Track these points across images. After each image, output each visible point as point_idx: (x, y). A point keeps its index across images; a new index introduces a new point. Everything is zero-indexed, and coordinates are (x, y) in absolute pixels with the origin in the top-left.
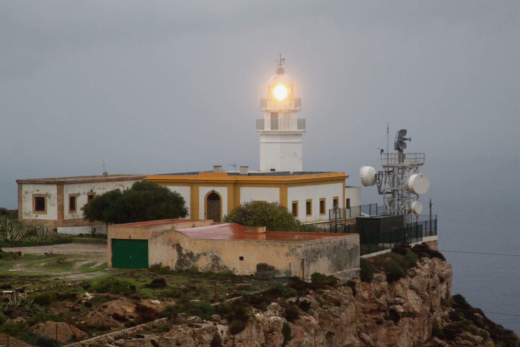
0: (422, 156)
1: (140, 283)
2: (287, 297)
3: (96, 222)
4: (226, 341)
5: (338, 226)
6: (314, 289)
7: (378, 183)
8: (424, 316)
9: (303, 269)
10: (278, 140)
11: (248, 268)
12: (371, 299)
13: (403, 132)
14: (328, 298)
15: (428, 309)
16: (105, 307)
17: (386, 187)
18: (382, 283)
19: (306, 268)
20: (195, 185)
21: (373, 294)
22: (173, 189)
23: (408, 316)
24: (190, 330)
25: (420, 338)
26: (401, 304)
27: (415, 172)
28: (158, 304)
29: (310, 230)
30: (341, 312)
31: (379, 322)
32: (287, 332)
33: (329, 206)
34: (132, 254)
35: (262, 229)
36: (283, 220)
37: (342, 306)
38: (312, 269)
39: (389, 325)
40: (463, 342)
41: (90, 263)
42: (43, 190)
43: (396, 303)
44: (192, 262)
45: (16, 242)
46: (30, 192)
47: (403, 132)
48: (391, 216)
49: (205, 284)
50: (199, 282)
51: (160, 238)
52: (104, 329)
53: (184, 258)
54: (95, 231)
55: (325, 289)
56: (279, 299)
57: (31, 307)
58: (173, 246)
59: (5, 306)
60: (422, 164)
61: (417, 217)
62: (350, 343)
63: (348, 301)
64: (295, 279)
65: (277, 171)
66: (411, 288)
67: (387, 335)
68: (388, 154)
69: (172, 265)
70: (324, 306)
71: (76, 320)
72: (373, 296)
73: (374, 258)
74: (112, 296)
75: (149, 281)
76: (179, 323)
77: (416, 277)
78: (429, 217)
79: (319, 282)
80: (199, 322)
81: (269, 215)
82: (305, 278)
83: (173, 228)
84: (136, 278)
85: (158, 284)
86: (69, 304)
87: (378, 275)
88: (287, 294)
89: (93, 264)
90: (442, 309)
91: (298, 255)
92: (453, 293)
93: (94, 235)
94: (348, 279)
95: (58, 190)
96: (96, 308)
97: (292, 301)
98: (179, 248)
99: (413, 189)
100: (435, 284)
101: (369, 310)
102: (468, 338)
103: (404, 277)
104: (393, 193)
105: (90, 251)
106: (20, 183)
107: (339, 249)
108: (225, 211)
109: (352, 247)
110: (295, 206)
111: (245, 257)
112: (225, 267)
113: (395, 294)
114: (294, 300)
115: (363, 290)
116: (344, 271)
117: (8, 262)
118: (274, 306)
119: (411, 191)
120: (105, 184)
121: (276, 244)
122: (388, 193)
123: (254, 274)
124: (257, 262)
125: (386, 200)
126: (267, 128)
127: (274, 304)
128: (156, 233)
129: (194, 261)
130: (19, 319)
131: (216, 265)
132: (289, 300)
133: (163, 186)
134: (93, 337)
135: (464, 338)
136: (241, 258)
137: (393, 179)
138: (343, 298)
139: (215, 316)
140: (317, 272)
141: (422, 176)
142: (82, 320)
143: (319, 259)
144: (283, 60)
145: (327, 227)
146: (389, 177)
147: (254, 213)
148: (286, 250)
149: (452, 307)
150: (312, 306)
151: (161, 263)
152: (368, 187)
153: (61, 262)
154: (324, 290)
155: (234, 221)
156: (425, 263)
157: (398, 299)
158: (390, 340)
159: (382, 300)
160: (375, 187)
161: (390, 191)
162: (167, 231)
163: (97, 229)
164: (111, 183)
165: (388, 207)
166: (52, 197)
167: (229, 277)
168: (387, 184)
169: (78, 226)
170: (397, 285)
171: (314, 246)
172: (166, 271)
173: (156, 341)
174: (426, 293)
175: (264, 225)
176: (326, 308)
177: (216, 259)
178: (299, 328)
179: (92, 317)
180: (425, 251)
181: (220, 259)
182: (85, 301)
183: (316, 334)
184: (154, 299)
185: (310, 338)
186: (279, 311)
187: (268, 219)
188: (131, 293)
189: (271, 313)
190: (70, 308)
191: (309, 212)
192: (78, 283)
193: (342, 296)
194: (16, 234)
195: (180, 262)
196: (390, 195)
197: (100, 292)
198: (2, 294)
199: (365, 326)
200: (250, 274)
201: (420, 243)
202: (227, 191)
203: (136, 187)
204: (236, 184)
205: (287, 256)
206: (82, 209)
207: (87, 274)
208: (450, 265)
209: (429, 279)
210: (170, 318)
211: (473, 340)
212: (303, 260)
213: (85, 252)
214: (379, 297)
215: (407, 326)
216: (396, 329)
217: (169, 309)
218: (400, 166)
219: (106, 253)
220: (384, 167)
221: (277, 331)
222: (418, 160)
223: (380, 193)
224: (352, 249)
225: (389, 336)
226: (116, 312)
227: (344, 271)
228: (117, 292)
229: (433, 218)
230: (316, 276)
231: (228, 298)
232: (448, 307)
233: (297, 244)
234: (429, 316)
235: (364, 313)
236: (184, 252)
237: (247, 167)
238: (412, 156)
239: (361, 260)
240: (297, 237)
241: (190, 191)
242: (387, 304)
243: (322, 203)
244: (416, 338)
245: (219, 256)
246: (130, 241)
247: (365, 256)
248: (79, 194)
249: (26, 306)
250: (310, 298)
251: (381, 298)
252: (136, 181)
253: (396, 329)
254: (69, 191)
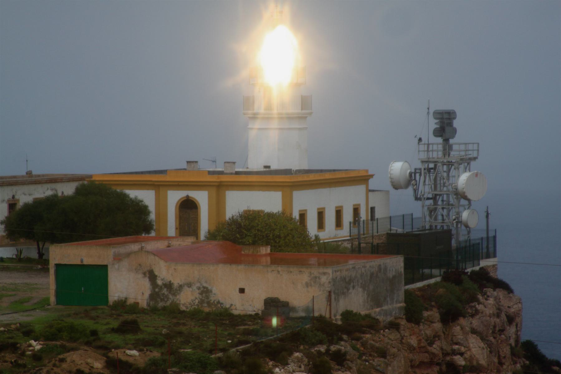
0: (476, 147)
2: (314, 345)
5: (362, 245)
6: (349, 333)
7: (413, 185)
9: (330, 305)
12: (420, 348)
14: (369, 347)
15: (496, 360)
16: (62, 360)
18: (434, 325)
19: (334, 304)
21: (423, 341)
22: (133, 193)
26: (462, 354)
27: (465, 171)
28: (135, 356)
29: (329, 252)
30: (387, 365)
33: (347, 217)
35: (265, 250)
36: (293, 237)
37: (388, 357)
43: (454, 353)
44: (171, 296)
50: (184, 324)
51: (125, 263)
53: (160, 290)
55: (364, 333)
56: (302, 347)
58: (144, 274)
60: (475, 159)
61: (469, 232)
63: (395, 350)
64: (321, 319)
66: (474, 331)
68: (428, 145)
70: (364, 357)
73: (420, 289)
74: (68, 344)
75: (115, 324)
77: (478, 317)
78: (485, 233)
79: (353, 325)
81: (274, 230)
82: (333, 318)
83: (142, 248)
84: (92, 318)
85: (129, 327)
87: (429, 313)
88: (313, 340)
91: (323, 285)
92: (524, 338)
93: (19, 259)
94: (389, 319)
96: (49, 362)
97: (319, 351)
98: (152, 277)
99: (464, 193)
101: (418, 363)
103: (464, 317)
104: (434, 198)
105: (18, 281)
109: (394, 274)
112: (219, 302)
113: (452, 340)
114: (323, 349)
115: (410, 335)
116: (385, 308)
118: (297, 358)
119: (461, 195)
122: (428, 199)
123: (260, 312)
124: (264, 296)
125: (426, 208)
127: (297, 354)
129: (174, 295)
131: (206, 300)
132: (316, 349)
133: (118, 190)
136: (242, 291)
138: (389, 347)
141: (477, 175)
145: (348, 245)
146: (430, 176)
148: (305, 277)
149: (525, 358)
150: (348, 357)
151: (126, 298)
152: (400, 191)
154: (362, 335)
155: (225, 238)
156: (488, 296)
157: (456, 347)
159: (435, 348)
160: (410, 190)
161: (430, 196)
162: (135, 253)
163: (23, 251)
165: (428, 218)
167: (225, 318)
168: (427, 187)
170: (454, 328)
172: (134, 308)
174: (491, 338)
175: (267, 244)
176: (366, 361)
177: (205, 292)
180: (485, 280)
181: (211, 291)
182: (30, 353)
186: (305, 365)
187: (273, 235)
188: (94, 340)
189: (294, 368)
190: (11, 363)
191: (321, 225)
195: (154, 296)
196: (431, 202)
200: (253, 313)
201: (477, 268)
204: (219, 186)
205: (307, 287)
207: (21, 314)
208: (520, 299)
209: (495, 319)
212: (330, 292)
213: (12, 284)
214: (431, 344)
218: (445, 161)
220: (423, 162)
222: (470, 152)
223: (417, 199)
224: (394, 277)
226: (78, 367)
228: (72, 339)
229: (491, 234)
230: (347, 315)
231: (233, 345)
232: (519, 358)
235: (412, 367)
236: (159, 282)
237: (234, 163)
238: (463, 147)
239: (407, 292)
241: (154, 196)
242: (443, 354)
243: (339, 213)
245: (209, 288)
250: (344, 346)
251: (434, 346)
252: (81, 182)
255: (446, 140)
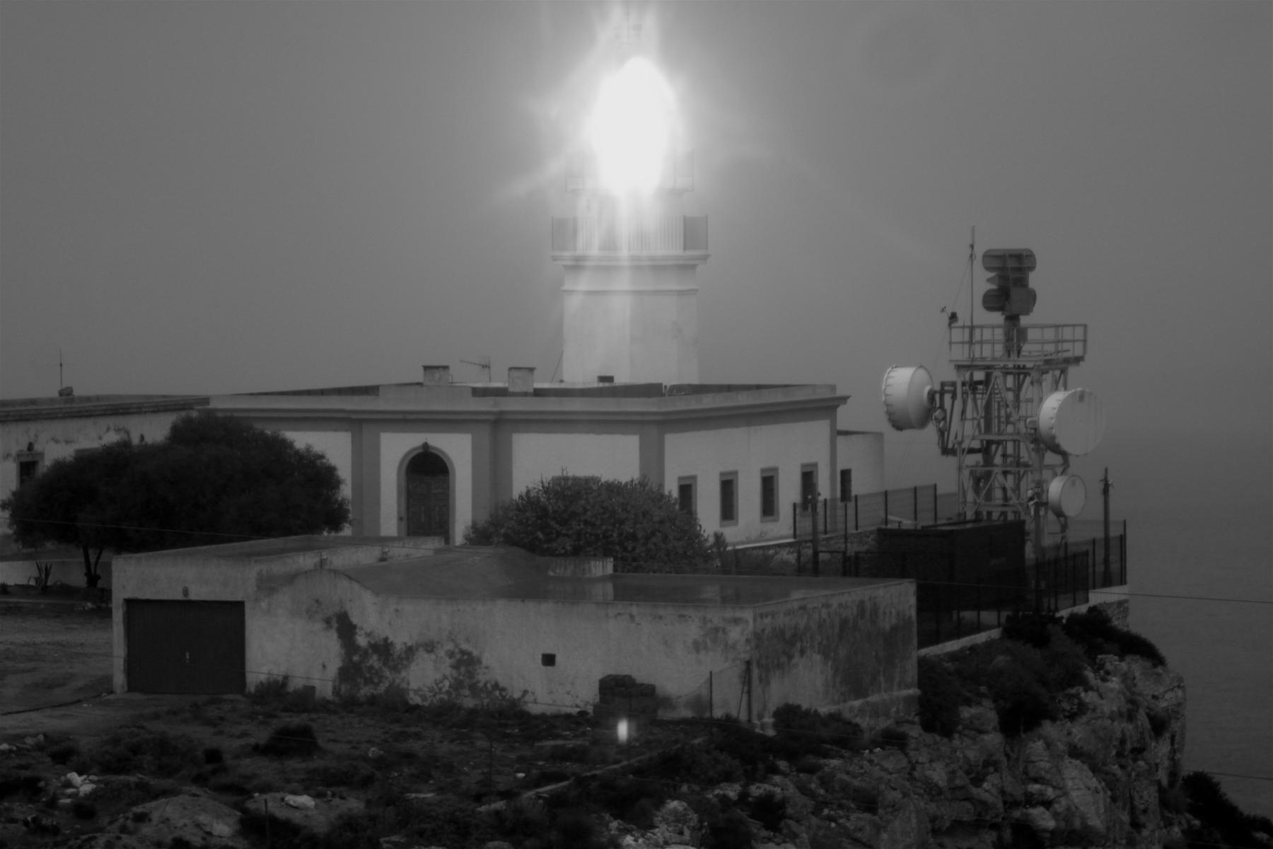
2: (712, 783)
3: (49, 545)
6: (791, 756)
7: (938, 421)
8: (1115, 841)
9: (749, 692)
12: (954, 789)
14: (837, 787)
15: (1126, 818)
16: (142, 818)
18: (986, 737)
19: (757, 689)
21: (960, 773)
22: (301, 439)
26: (1047, 804)
27: (1055, 388)
28: (307, 808)
29: (747, 570)
30: (878, 829)
33: (789, 493)
35: (602, 568)
36: (665, 538)
37: (880, 811)
38: (779, 692)
43: (1030, 800)
44: (387, 673)
48: (983, 524)
50: (418, 736)
53: (364, 659)
54: (47, 574)
56: (685, 788)
58: (328, 621)
60: (1078, 360)
61: (1064, 527)
63: (897, 795)
64: (728, 724)
70: (826, 811)
73: (953, 656)
74: (154, 782)
75: (261, 735)
77: (1084, 719)
78: (1102, 528)
79: (800, 738)
81: (622, 522)
82: (756, 721)
83: (322, 563)
87: (974, 711)
88: (711, 773)
90: (1163, 817)
91: (734, 647)
92: (1189, 767)
93: (43, 589)
94: (883, 724)
96: (111, 823)
97: (724, 796)
98: (345, 628)
99: (1053, 438)
101: (948, 824)
103: (1054, 719)
104: (986, 450)
105: (40, 638)
108: (464, 510)
109: (894, 621)
112: (496, 686)
113: (1026, 773)
114: (732, 791)
115: (931, 761)
116: (873, 698)
118: (675, 811)
119: (1045, 443)
120: (73, 426)
121: (661, 612)
122: (971, 451)
123: (590, 709)
124: (599, 673)
125: (966, 473)
127: (674, 804)
129: (395, 669)
132: (717, 792)
133: (268, 432)
136: (549, 660)
138: (882, 787)
140: (793, 700)
145: (789, 557)
148: (693, 630)
150: (790, 811)
151: (286, 678)
152: (907, 433)
154: (822, 761)
155: (510, 541)
156: (1108, 673)
157: (1034, 788)
159: (988, 790)
160: (931, 431)
161: (976, 444)
165: (970, 496)
167: (510, 721)
168: (968, 425)
172: (305, 700)
174: (1115, 768)
176: (831, 819)
177: (466, 662)
180: (1100, 634)
181: (479, 661)
182: (68, 801)
184: (295, 793)
186: (693, 829)
187: (620, 535)
188: (214, 772)
189: (667, 835)
190: (26, 823)
191: (728, 511)
192: (30, 741)
193: (880, 779)
195: (349, 672)
196: (978, 457)
197: (118, 771)
200: (575, 711)
201: (1082, 609)
202: (637, 444)
203: (179, 434)
204: (498, 423)
205: (698, 651)
207: (48, 712)
208: (1181, 680)
209: (1124, 725)
212: (748, 663)
213: (26, 644)
214: (978, 781)
218: (1010, 365)
220: (959, 367)
222: (1066, 346)
223: (946, 451)
224: (894, 629)
226: (178, 834)
227: (873, 698)
229: (1115, 532)
230: (787, 715)
233: (729, 613)
235: (935, 832)
236: (362, 641)
237: (531, 370)
238: (1050, 334)
239: (922, 662)
242: (1005, 803)
243: (769, 484)
245: (475, 653)
246: (187, 605)
247: (924, 651)
250: (780, 786)
251: (985, 785)
252: (183, 414)
255: (1012, 319)
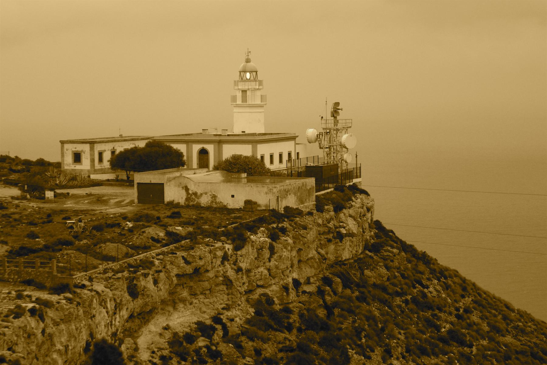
1: (163, 214)
2: (270, 224)
4: (232, 256)
10: (248, 110)
11: (238, 203)
13: (337, 104)
16: (144, 232)
17: (325, 143)
20: (190, 143)
22: (175, 146)
23: (349, 236)
24: (208, 249)
25: (357, 251)
26: (344, 228)
29: (277, 175)
30: (307, 234)
31: (329, 241)
32: (272, 249)
34: (152, 194)
35: (244, 175)
38: (284, 203)
39: (337, 243)
40: (385, 254)
41: (121, 201)
42: (79, 148)
45: (63, 186)
46: (70, 149)
47: (337, 104)
49: (207, 215)
50: (204, 214)
52: (146, 248)
53: (191, 196)
55: (296, 217)
57: (91, 232)
58: (183, 188)
59: (71, 232)
60: (350, 127)
61: (347, 165)
62: (312, 256)
63: (311, 226)
64: (273, 210)
65: (246, 132)
66: (350, 216)
67: (335, 249)
69: (182, 201)
71: (125, 242)
72: (325, 222)
73: (323, 195)
75: (169, 213)
76: (199, 244)
80: (212, 243)
83: (181, 174)
84: (157, 211)
85: (175, 215)
86: (118, 230)
89: (123, 201)
94: (308, 210)
95: (90, 147)
98: (187, 189)
100: (365, 213)
102: (389, 251)
103: (345, 208)
104: (329, 148)
105: (117, 191)
106: (63, 143)
107: (302, 188)
110: (262, 157)
111: (235, 195)
112: (221, 202)
117: (61, 200)
119: (343, 146)
122: (326, 148)
124: (244, 199)
126: (239, 102)
127: (262, 229)
128: (170, 178)
129: (198, 198)
130: (85, 241)
134: (140, 254)
135: (386, 251)
136: (233, 196)
137: (330, 138)
139: (223, 238)
142: (130, 242)
143: (289, 196)
144: (250, 52)
147: (237, 163)
148: (265, 189)
153: (100, 200)
157: (341, 224)
158: (337, 253)
159: (331, 225)
160: (317, 143)
161: (327, 146)
164: (127, 142)
165: (326, 158)
166: (86, 153)
167: (224, 210)
169: (105, 173)
171: (285, 187)
172: (178, 205)
173: (185, 256)
175: (245, 172)
177: (214, 197)
178: (280, 246)
179: (136, 240)
180: (355, 189)
183: (292, 250)
185: (288, 253)
191: (272, 162)
194: (62, 179)
195: (187, 199)
196: (328, 149)
198: (66, 223)
199: (320, 243)
201: (351, 184)
203: (147, 145)
204: (219, 142)
206: (108, 161)
210: (192, 240)
211: (392, 252)
214: (329, 223)
215: (348, 243)
216: (341, 246)
217: (190, 233)
219: (133, 193)
221: (265, 248)
223: (320, 148)
224: (310, 189)
225: (336, 250)
228: (148, 221)
229: (359, 166)
230: (287, 208)
233: (273, 186)
234: (363, 236)
236: (190, 192)
238: (344, 121)
239: (316, 196)
240: (268, 181)
243: (281, 156)
244: (354, 252)
248: (105, 151)
249: (87, 232)
250: (286, 224)
253: (341, 246)
254: (98, 148)
